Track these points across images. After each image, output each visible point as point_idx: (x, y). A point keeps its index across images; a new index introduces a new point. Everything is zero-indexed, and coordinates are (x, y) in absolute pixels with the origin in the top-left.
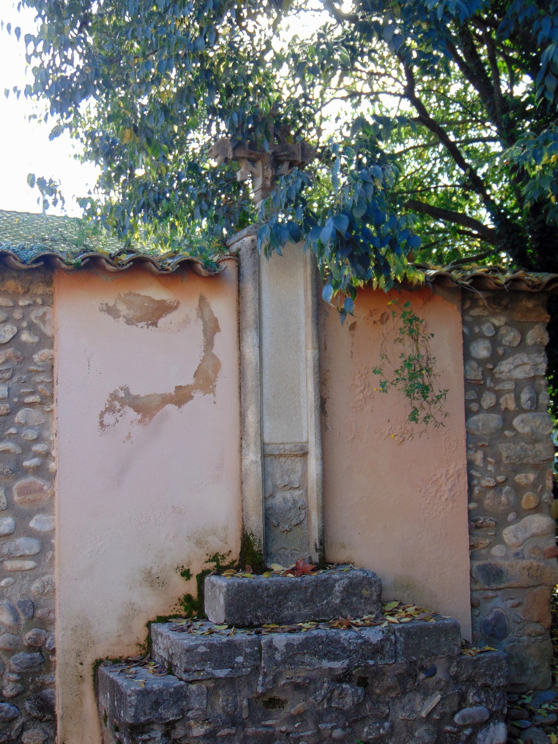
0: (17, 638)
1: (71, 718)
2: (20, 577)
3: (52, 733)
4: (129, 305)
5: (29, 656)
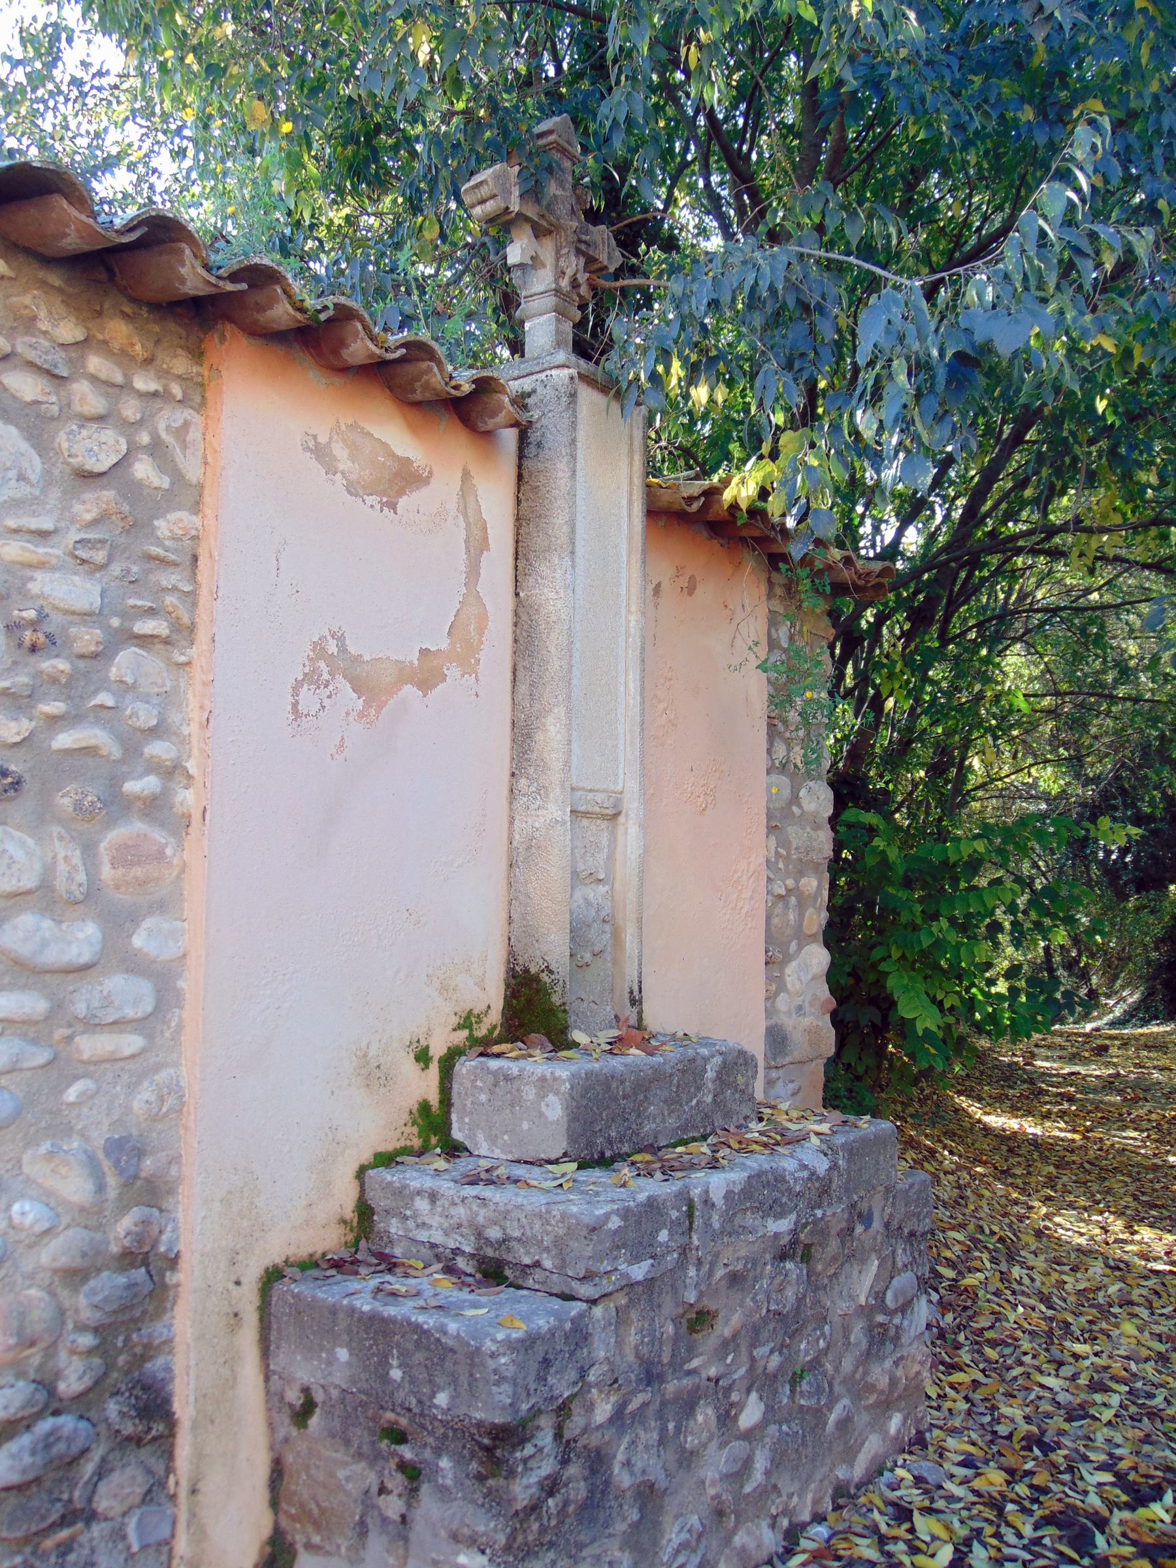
0: (98, 1236)
1: (212, 1422)
2: (109, 1077)
3: (160, 1468)
4: (355, 451)
5: (122, 1280)
